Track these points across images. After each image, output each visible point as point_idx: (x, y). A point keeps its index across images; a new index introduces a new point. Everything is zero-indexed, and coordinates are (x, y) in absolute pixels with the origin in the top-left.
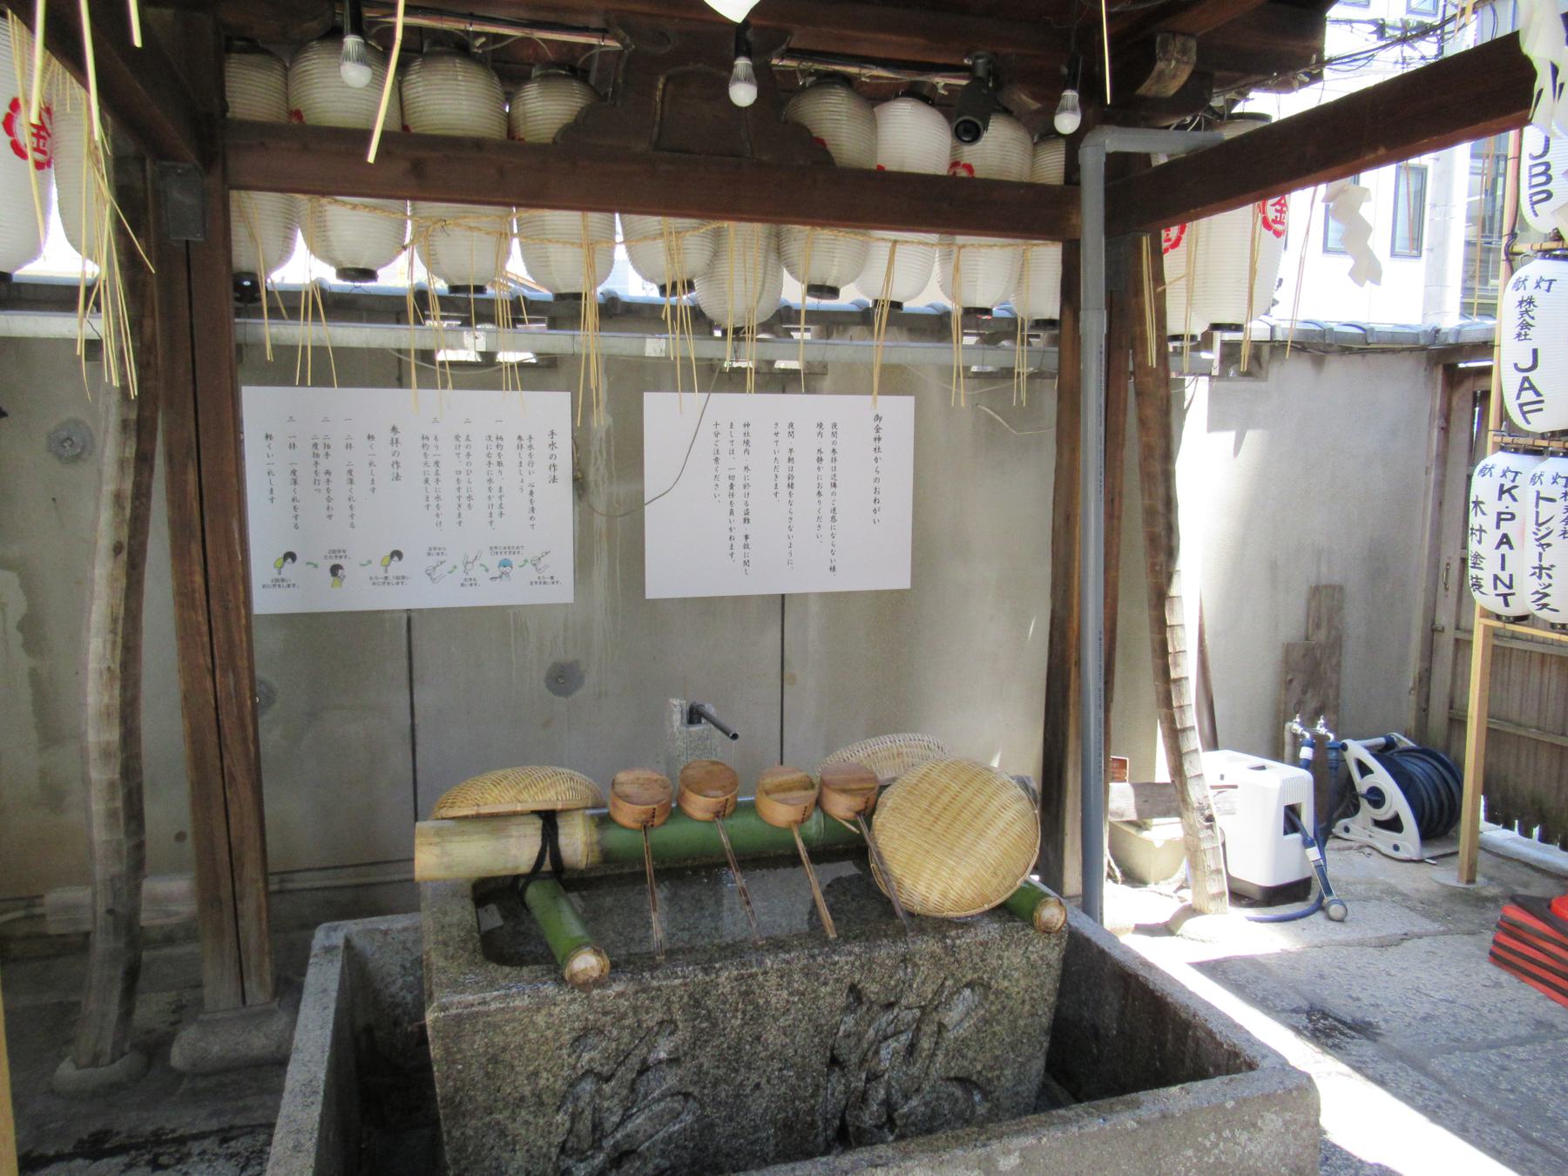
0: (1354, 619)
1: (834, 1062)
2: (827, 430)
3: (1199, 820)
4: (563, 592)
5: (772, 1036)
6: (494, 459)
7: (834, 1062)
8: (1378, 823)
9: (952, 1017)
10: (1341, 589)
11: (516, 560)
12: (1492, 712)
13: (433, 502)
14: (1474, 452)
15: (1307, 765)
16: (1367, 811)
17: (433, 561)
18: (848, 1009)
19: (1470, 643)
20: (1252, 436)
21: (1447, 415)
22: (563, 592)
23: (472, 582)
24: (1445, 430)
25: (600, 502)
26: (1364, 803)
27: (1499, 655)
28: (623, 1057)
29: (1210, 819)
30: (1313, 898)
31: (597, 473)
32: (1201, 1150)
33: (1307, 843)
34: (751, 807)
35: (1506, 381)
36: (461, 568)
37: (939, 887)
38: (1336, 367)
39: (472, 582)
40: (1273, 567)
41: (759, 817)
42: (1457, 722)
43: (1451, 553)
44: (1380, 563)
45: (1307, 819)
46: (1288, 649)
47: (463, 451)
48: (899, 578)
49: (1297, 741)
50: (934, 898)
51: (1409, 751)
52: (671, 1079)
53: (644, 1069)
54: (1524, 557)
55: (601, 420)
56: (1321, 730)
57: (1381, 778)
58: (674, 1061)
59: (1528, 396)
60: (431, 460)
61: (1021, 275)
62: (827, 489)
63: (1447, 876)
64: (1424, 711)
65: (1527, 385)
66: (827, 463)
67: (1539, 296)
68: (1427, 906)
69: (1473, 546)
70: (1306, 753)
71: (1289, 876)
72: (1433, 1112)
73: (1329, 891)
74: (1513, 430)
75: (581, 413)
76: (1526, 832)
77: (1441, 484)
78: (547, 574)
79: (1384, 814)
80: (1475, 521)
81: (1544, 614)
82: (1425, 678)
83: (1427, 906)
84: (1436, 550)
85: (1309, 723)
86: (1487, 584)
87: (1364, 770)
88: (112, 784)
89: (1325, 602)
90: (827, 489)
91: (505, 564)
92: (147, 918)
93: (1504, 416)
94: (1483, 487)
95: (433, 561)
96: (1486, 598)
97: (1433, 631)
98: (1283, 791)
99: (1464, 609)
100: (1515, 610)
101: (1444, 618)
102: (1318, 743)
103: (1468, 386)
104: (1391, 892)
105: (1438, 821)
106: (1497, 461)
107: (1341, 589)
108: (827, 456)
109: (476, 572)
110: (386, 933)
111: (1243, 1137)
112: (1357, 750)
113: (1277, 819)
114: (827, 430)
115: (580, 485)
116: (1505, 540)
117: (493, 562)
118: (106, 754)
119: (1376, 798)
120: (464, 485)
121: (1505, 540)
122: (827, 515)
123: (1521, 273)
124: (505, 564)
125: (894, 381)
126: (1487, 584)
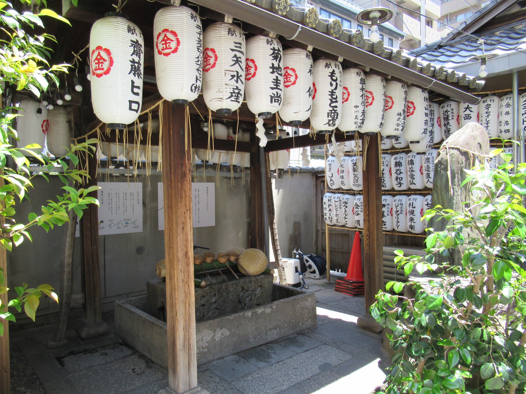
0: (302, 228)
1: (240, 302)
2: (197, 190)
3: (281, 269)
4: (140, 230)
5: (230, 297)
6: (125, 198)
7: (240, 302)
8: (311, 272)
9: (257, 292)
10: (299, 223)
11: (129, 222)
12: (330, 248)
13: (110, 209)
14: (323, 193)
15: (298, 258)
16: (309, 270)
17: (110, 223)
18: (242, 292)
19: (325, 233)
20: (281, 190)
21: (316, 185)
22: (140, 230)
23: (119, 228)
24: (316, 189)
25: (148, 207)
26: (308, 269)
27: (330, 235)
28: (208, 301)
29: (283, 268)
30: (301, 286)
31: (148, 201)
32: (300, 304)
33: (300, 274)
34: (217, 260)
35: (328, 179)
36: (116, 225)
37: (254, 269)
38: (296, 176)
39: (119, 228)
40: (287, 219)
41: (218, 262)
42: (324, 250)
43: (320, 214)
44: (306, 217)
45: (299, 269)
46: (291, 236)
47: (118, 196)
48: (213, 223)
49: (295, 254)
50: (253, 271)
51: (315, 257)
52: (215, 306)
53: (211, 304)
54: (334, 213)
55: (149, 188)
56: (300, 252)
57: (311, 262)
58: (215, 302)
59: (332, 182)
60: (110, 199)
61: (242, 158)
62: (197, 204)
63: (326, 281)
64: (317, 248)
65: (331, 180)
66: (197, 198)
67: (332, 163)
68: (323, 285)
69: (325, 211)
70: (297, 256)
71: (297, 282)
72: (330, 309)
73: (305, 283)
74: (329, 188)
75: (144, 187)
76: (338, 271)
77: (316, 199)
78: (136, 225)
79: (312, 270)
80: (324, 206)
81: (338, 224)
82: (317, 241)
83: (323, 285)
84: (317, 214)
85: (297, 250)
86: (328, 219)
87: (307, 261)
88: (69, 272)
89: (297, 226)
90: (197, 204)
91: (127, 223)
92: (72, 304)
93: (328, 186)
94: (325, 200)
95: (110, 223)
96: (328, 222)
97: (317, 231)
98: (295, 263)
99: (323, 225)
100: (333, 224)
101: (319, 228)
102: (299, 254)
103: (320, 180)
104: (315, 284)
105: (322, 271)
106: (327, 194)
107: (299, 223)
108: (197, 196)
109: (120, 225)
110: (131, 300)
111: (306, 302)
112: (305, 257)
113: (293, 270)
114: (197, 190)
115: (144, 204)
116: (330, 210)
117: (124, 223)
118: (69, 265)
119: (310, 267)
120: (118, 204)
121: (330, 210)
122: (197, 210)
123: (328, 159)
124: (127, 223)
125: (210, 179)
126: (328, 219)
